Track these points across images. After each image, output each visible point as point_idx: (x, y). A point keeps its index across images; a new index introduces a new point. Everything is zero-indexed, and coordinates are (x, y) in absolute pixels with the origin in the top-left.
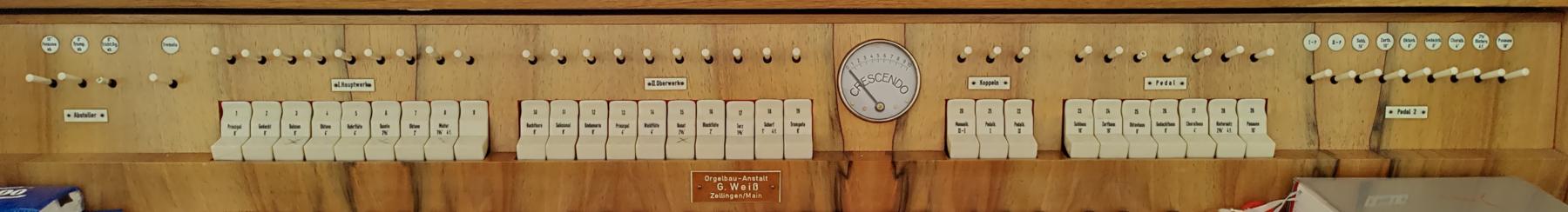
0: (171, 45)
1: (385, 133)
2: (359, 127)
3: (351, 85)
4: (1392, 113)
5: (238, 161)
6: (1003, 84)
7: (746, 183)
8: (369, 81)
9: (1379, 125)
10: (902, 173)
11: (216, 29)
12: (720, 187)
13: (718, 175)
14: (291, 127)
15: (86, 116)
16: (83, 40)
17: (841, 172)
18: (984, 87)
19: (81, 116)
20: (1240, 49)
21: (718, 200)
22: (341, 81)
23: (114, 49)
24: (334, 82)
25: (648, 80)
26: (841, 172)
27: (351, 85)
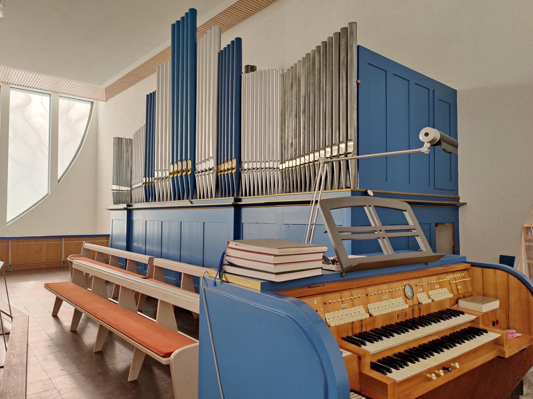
24: (341, 305)
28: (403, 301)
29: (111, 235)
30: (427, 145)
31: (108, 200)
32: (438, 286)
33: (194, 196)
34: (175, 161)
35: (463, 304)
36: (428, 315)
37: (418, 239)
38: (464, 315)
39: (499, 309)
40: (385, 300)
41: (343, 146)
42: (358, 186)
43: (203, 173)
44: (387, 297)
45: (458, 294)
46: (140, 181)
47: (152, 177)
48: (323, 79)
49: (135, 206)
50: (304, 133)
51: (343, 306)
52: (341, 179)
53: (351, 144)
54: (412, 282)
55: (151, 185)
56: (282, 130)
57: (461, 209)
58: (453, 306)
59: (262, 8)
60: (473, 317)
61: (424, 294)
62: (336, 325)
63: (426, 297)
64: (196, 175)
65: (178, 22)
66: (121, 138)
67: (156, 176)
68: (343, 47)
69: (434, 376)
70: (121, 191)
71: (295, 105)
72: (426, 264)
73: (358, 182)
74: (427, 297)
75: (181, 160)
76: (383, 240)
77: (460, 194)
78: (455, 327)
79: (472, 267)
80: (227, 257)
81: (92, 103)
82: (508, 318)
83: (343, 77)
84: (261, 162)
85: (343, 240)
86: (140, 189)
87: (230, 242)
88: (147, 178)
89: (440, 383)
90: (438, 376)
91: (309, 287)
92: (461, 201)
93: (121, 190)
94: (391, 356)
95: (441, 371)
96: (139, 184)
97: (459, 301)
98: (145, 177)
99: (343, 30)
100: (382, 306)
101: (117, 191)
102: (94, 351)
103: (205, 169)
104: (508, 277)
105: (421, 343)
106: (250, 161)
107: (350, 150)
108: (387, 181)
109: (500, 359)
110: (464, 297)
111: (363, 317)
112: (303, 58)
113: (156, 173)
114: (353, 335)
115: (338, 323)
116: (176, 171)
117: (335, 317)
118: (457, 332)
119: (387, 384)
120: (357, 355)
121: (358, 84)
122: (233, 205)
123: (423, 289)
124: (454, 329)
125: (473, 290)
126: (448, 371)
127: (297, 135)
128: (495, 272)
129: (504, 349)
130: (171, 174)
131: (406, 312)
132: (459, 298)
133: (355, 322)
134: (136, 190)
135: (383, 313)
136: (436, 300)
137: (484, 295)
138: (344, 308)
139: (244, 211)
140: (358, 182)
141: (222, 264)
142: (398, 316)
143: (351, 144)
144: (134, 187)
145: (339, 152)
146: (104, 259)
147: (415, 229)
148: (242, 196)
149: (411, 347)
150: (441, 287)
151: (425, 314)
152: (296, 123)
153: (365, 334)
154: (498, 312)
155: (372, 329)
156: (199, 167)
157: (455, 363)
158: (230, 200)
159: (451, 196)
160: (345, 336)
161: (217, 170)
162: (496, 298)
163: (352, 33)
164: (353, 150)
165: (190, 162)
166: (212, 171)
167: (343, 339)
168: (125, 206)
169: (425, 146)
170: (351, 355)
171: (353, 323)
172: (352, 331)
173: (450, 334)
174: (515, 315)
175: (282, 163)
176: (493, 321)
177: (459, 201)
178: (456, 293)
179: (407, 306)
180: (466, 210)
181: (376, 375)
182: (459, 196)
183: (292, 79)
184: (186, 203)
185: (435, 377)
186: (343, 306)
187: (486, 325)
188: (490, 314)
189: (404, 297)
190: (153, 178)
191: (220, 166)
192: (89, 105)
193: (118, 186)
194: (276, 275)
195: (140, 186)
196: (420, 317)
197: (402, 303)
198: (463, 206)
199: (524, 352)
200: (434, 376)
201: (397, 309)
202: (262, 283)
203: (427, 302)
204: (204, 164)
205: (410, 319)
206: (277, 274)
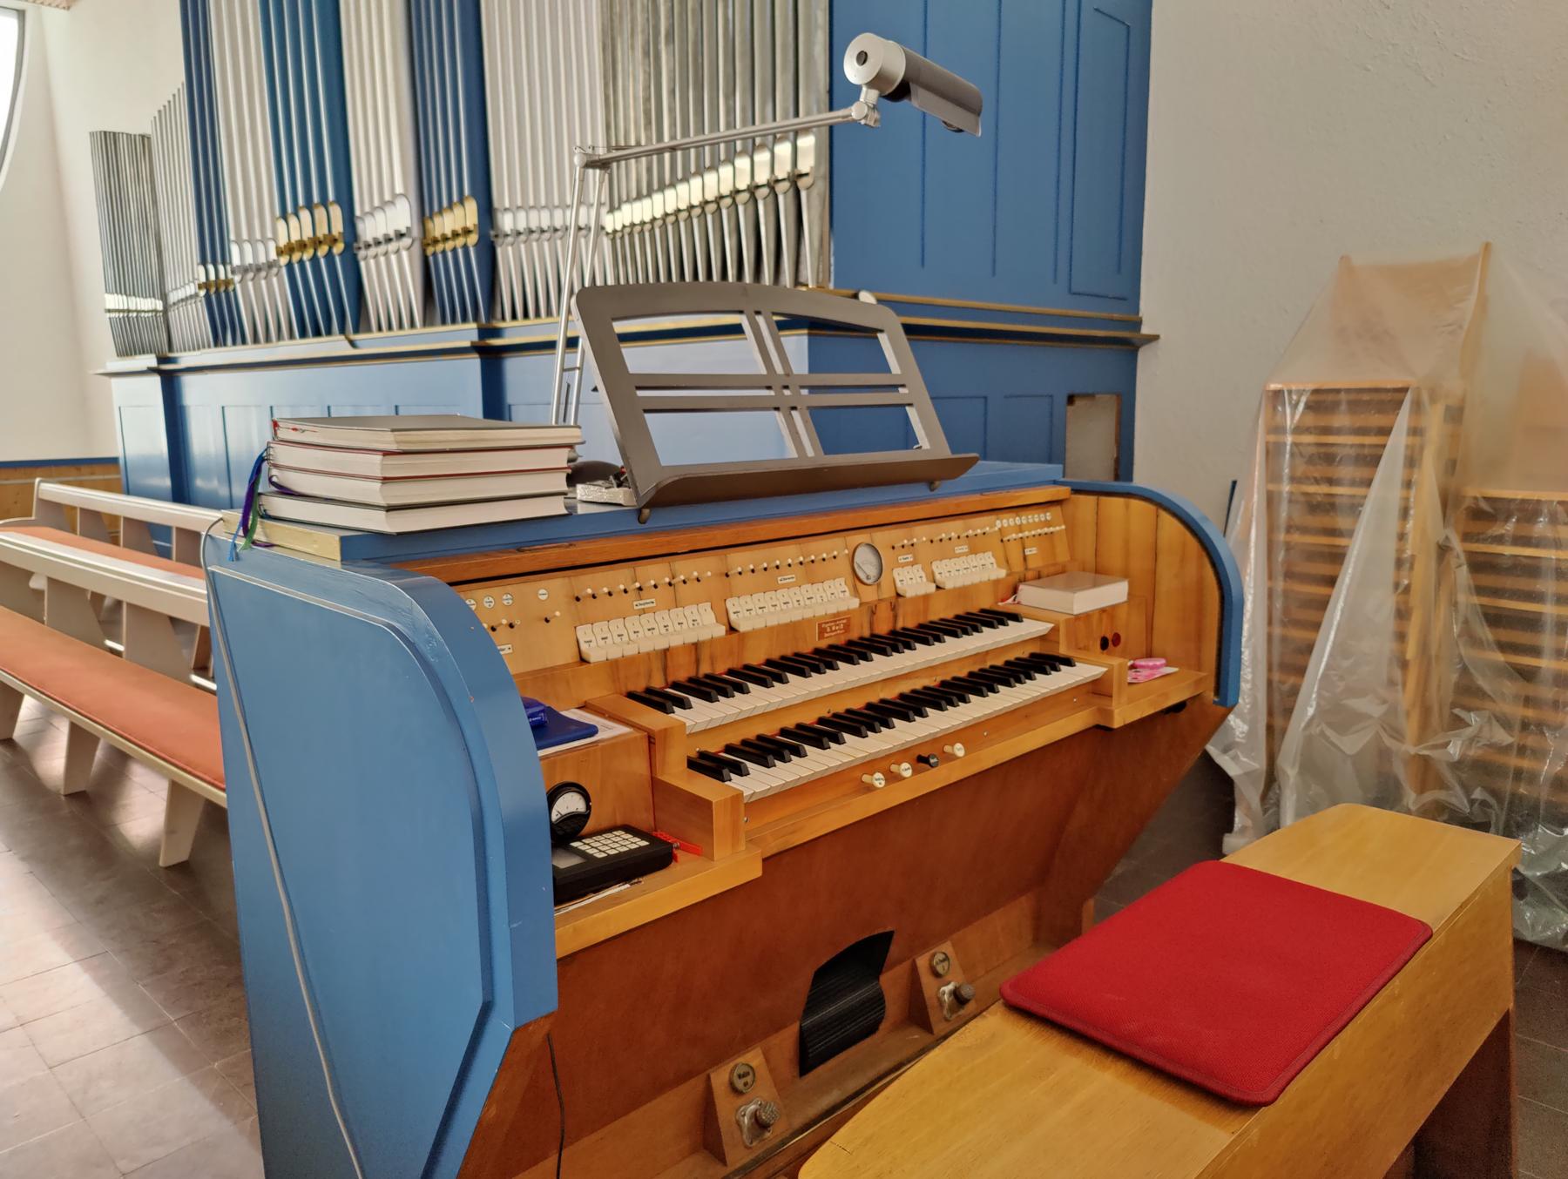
0: (543, 594)
1: (667, 630)
2: (654, 629)
3: (644, 604)
4: (1028, 552)
6: (910, 558)
9: (1025, 558)
11: (567, 580)
12: (828, 630)
13: (828, 623)
14: (603, 639)
16: (491, 599)
21: (827, 637)
24: (635, 603)
25: (779, 578)
27: (644, 604)
28: (847, 589)
29: (121, 462)
30: (869, 96)
31: (102, 340)
32: (965, 549)
33: (362, 325)
34: (290, 208)
35: (1029, 595)
36: (921, 626)
37: (912, 413)
38: (1022, 621)
39: (1126, 604)
40: (788, 586)
42: (829, 280)
43: (382, 249)
44: (794, 580)
45: (1026, 569)
46: (191, 279)
47: (224, 263)
49: (186, 359)
50: (672, 110)
51: (641, 605)
52: (802, 267)
54: (881, 537)
55: (217, 292)
56: (610, 104)
57: (1144, 355)
58: (1003, 601)
60: (1042, 628)
61: (917, 572)
62: (609, 658)
63: (921, 577)
64: (362, 254)
66: (114, 134)
67: (236, 261)
69: (878, 780)
70: (135, 314)
72: (931, 483)
73: (832, 268)
74: (924, 579)
75: (309, 206)
76: (791, 414)
78: (987, 652)
79: (1073, 496)
80: (274, 472)
82: (1150, 628)
84: (550, 207)
85: (646, 411)
86: (194, 305)
87: (279, 424)
89: (900, 795)
90: (892, 778)
91: (520, 550)
92: (1145, 330)
93: (133, 311)
94: (769, 734)
95: (905, 765)
97: (1021, 587)
98: (204, 262)
100: (774, 603)
101: (121, 315)
103: (385, 235)
105: (874, 699)
106: (518, 208)
107: (806, 165)
109: (1100, 731)
110: (1039, 577)
111: (704, 636)
113: (235, 249)
115: (615, 654)
116: (296, 241)
117: (609, 635)
118: (992, 667)
119: (709, 803)
122: (477, 349)
123: (915, 557)
124: (985, 662)
125: (1071, 559)
126: (928, 766)
128: (1127, 507)
129: (1111, 706)
130: (282, 252)
132: (1023, 580)
133: (677, 648)
134: (181, 309)
136: (949, 585)
137: (1097, 571)
138: (644, 611)
139: (513, 367)
140: (832, 268)
141: (252, 494)
142: (822, 632)
144: (173, 298)
146: (101, 528)
147: (903, 386)
148: (503, 318)
149: (840, 709)
150: (973, 551)
151: (911, 624)
152: (647, 76)
153: (708, 681)
154: (1122, 614)
155: (735, 666)
156: (370, 229)
157: (952, 745)
158: (466, 333)
160: (639, 687)
161: (421, 236)
162: (1125, 575)
165: (336, 212)
166: (407, 241)
167: (632, 695)
168: (150, 361)
169: (862, 99)
170: (631, 733)
171: (666, 651)
172: (665, 674)
173: (971, 674)
174: (1166, 620)
175: (612, 210)
177: (1140, 329)
178: (1018, 567)
179: (854, 603)
181: (703, 786)
182: (1140, 315)
184: (334, 345)
185: (883, 783)
186: (641, 605)
187: (1082, 645)
188: (1095, 620)
190: (229, 268)
191: (429, 225)
193: (125, 297)
194: (387, 511)
195: (191, 297)
196: (893, 632)
197: (841, 595)
199: (1183, 715)
200: (878, 780)
201: (820, 612)
202: (343, 539)
203: (922, 592)
204: (379, 215)
205: (862, 638)
206: (390, 509)
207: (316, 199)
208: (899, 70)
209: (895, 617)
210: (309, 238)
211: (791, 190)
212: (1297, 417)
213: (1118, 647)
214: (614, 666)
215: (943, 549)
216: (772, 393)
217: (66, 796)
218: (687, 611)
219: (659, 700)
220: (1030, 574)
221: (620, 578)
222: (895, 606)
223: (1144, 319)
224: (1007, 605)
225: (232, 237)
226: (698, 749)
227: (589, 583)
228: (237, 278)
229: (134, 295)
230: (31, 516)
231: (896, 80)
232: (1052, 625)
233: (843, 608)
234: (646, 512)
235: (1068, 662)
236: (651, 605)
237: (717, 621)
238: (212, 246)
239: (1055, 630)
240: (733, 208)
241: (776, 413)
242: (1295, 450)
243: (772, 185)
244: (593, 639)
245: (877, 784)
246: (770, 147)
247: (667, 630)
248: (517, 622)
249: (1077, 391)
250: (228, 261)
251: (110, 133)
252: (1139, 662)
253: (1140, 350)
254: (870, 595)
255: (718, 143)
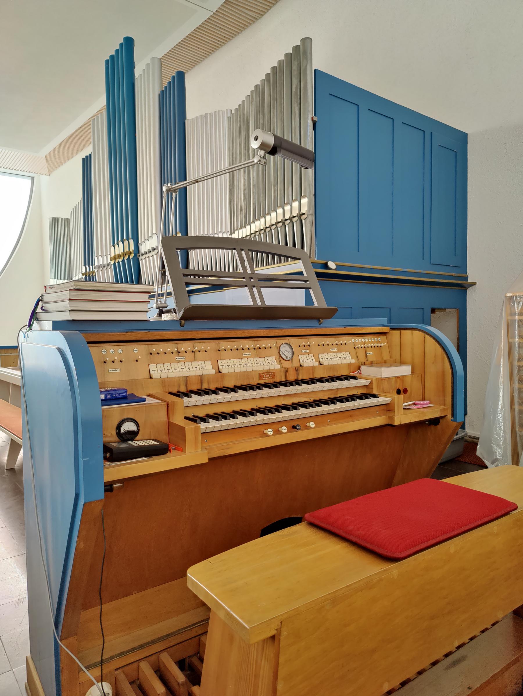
1: (190, 370)
2: (183, 369)
3: (180, 358)
4: (368, 354)
5: (214, 374)
6: (308, 351)
7: (269, 375)
8: (184, 357)
9: (366, 356)
10: (297, 370)
12: (264, 376)
14: (160, 370)
15: (115, 370)
16: (113, 350)
17: (286, 371)
18: (305, 352)
19: (114, 370)
20: (223, 347)
21: (264, 379)
22: (178, 357)
23: (122, 352)
24: (176, 358)
25: (243, 354)
26: (286, 371)
27: (180, 358)
28: (276, 361)
35: (365, 370)
41: (296, 204)
42: (315, 257)
43: (147, 255)
48: (274, 118)
53: (305, 201)
54: (293, 341)
57: (469, 291)
58: (353, 373)
59: (233, 37)
60: (366, 382)
64: (140, 258)
65: (112, 57)
66: (57, 218)
67: (96, 264)
68: (295, 73)
71: (244, 155)
77: (470, 272)
81: (33, 178)
82: (423, 387)
83: (295, 113)
88: (87, 267)
90: (277, 432)
92: (469, 280)
96: (79, 275)
97: (362, 367)
98: (85, 265)
99: (295, 49)
102: (5, 468)
104: (424, 337)
108: (359, 252)
111: (205, 373)
112: (252, 91)
113: (96, 259)
114: (187, 390)
115: (164, 376)
120: (165, 403)
121: (314, 124)
127: (247, 196)
131: (274, 373)
132: (364, 364)
135: (238, 370)
136: (325, 363)
143: (305, 201)
145: (292, 213)
150: (340, 351)
156: (144, 248)
159: (454, 274)
160: (175, 391)
163: (305, 52)
164: (307, 210)
165: (132, 242)
167: (171, 393)
174: (431, 384)
176: (397, 388)
177: (467, 281)
179: (278, 367)
180: (475, 291)
181: (189, 426)
182: (467, 274)
183: (240, 121)
188: (393, 381)
189: (278, 357)
192: (29, 181)
193: (57, 280)
197: (273, 363)
198: (472, 287)
200: (270, 432)
203: (311, 365)
207: (125, 238)
208: (271, 141)
209: (298, 374)
210: (121, 253)
211: (299, 220)
212: (520, 307)
213: (406, 394)
214: (163, 382)
215: (326, 349)
216: (245, 280)
217: (6, 470)
218: (200, 363)
219: (179, 395)
220: (367, 363)
221: (170, 347)
222: (297, 369)
223: (469, 276)
224: (355, 374)
225: (95, 255)
226: (193, 414)
227: (155, 347)
228: (96, 270)
229: (60, 279)
230: (17, 367)
231: (271, 147)
232: (370, 381)
233: (272, 368)
234: (183, 322)
235: (375, 396)
236: (183, 359)
237: (213, 369)
238: (88, 259)
239: (371, 383)
240: (276, 229)
241: (246, 288)
242: (520, 323)
243: (291, 219)
244: (156, 370)
245: (269, 433)
246: (291, 204)
247: (252, 365)
248: (123, 360)
249: (436, 307)
250: (94, 264)
251: (56, 218)
252: (417, 402)
253: (468, 289)
254: (286, 365)
255: (202, 176)
